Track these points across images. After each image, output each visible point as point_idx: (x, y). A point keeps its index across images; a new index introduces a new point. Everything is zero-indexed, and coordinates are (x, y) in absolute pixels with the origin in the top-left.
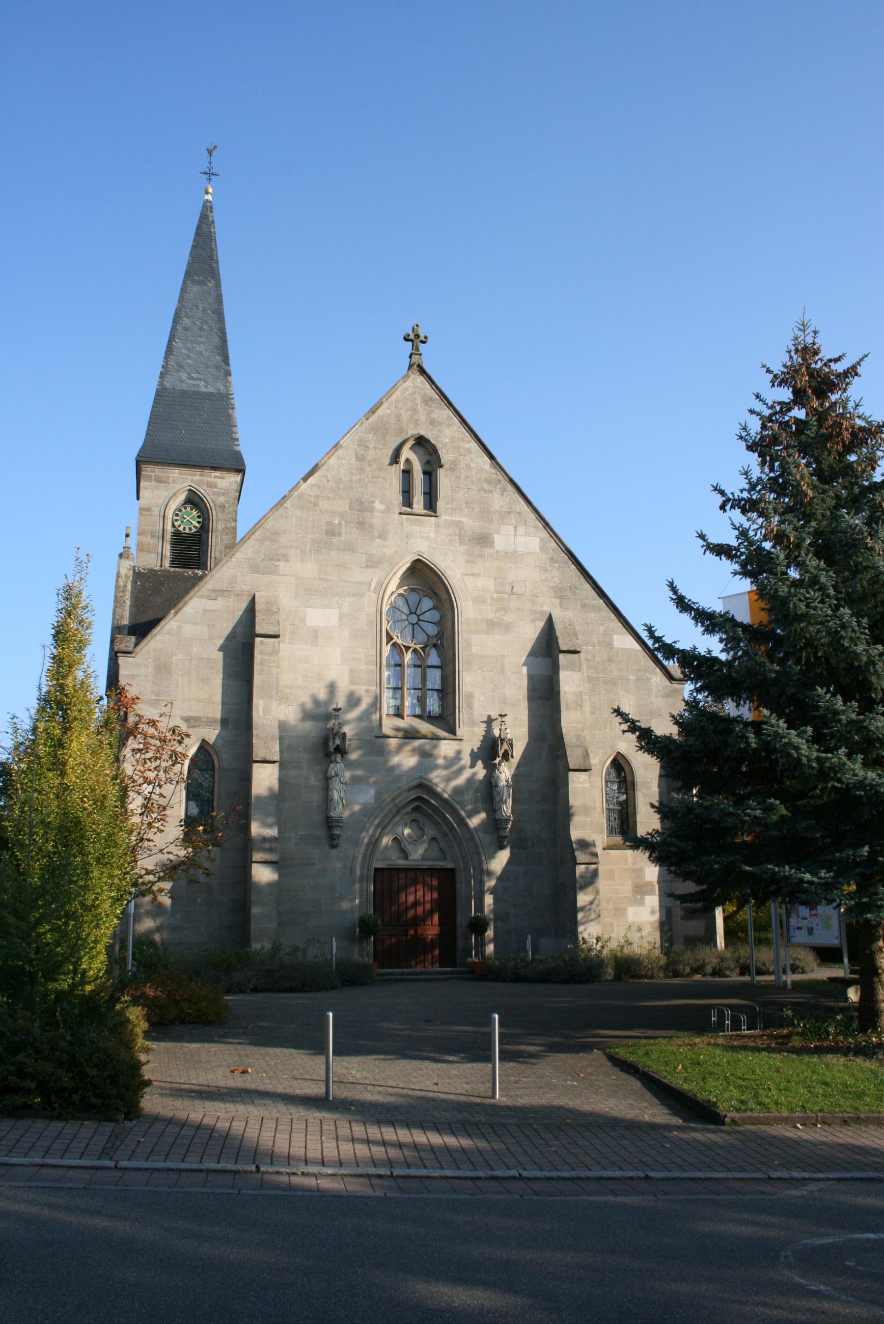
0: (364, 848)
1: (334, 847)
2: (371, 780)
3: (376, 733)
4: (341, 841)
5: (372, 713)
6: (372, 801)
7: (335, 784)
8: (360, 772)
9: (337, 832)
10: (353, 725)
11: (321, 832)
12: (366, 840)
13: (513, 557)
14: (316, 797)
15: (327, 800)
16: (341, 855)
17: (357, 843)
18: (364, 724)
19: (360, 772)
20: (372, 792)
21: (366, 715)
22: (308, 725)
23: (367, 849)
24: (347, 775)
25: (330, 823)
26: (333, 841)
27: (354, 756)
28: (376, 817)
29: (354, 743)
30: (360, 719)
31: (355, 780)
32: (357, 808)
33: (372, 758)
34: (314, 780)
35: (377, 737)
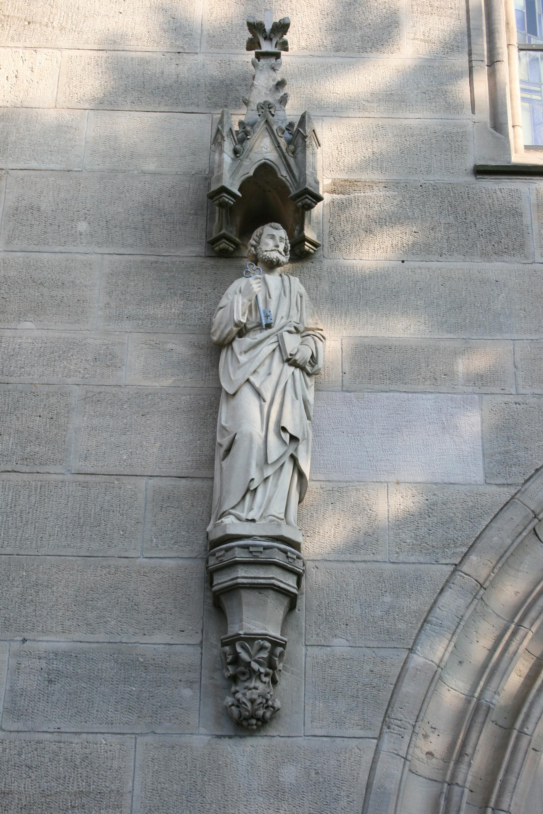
0: (437, 743)
1: (248, 722)
2: (462, 366)
3: (478, 154)
4: (293, 691)
5: (456, 76)
6: (476, 474)
7: (255, 366)
8: (402, 329)
9: (259, 619)
10: (356, 124)
11: (175, 641)
12: (452, 693)
13: (228, 670)
14: (156, 448)
15: (211, 445)
16: (290, 774)
17: (388, 706)
18: (419, 118)
19: (402, 329)
20: (472, 423)
21: (431, 81)
22: (133, 126)
23: (457, 753)
24: (334, 343)
25: (231, 582)
26: (242, 690)
27: (372, 254)
28: (505, 561)
29: (375, 198)
30: (392, 98)
31: (378, 367)
32: (391, 503)
33: (457, 266)
34: (145, 363)
35: (481, 171)
